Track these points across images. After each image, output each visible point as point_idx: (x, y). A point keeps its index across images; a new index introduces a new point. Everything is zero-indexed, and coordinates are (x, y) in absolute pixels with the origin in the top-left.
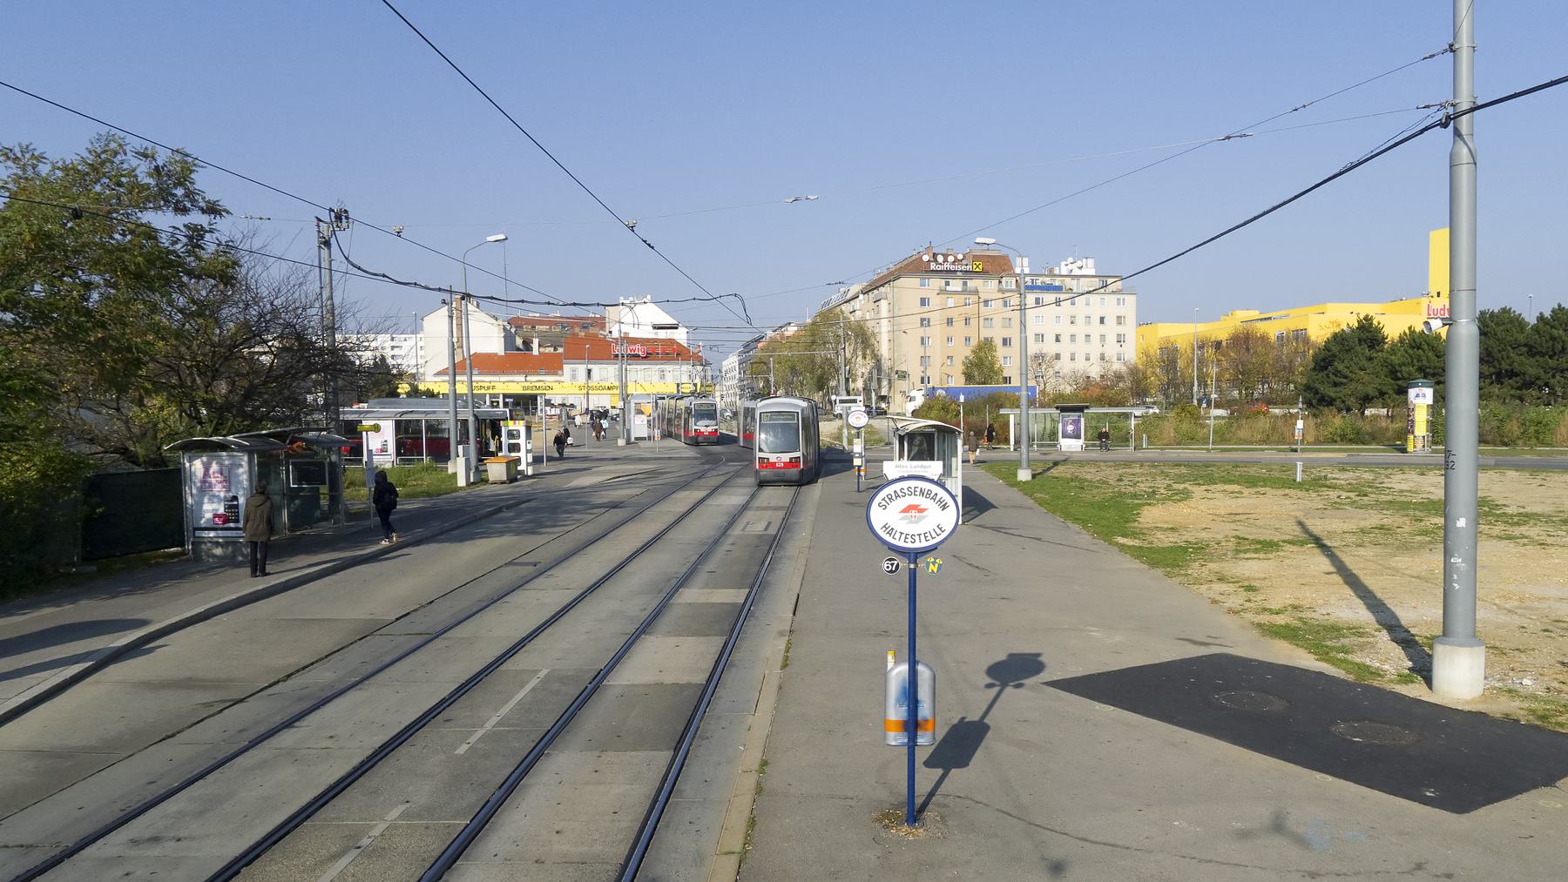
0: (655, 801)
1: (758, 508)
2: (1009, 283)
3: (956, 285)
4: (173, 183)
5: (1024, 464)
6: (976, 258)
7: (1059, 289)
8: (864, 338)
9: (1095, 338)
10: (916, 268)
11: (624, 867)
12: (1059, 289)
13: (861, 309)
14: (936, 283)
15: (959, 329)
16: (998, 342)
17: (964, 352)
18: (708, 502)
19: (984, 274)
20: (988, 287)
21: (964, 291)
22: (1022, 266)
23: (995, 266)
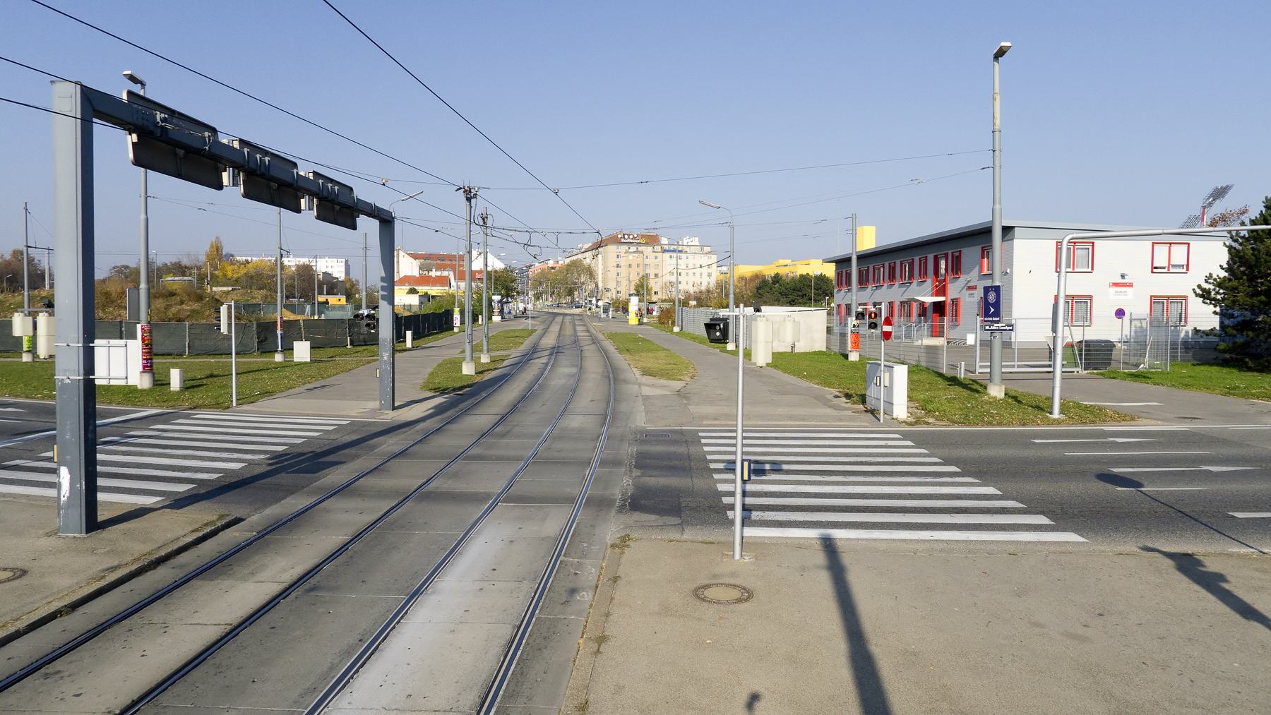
0: (372, 653)
1: (519, 459)
2: (658, 248)
3: (633, 249)
4: (692, 439)
5: (997, 378)
6: (643, 236)
7: (680, 251)
8: (591, 273)
9: (698, 274)
10: (615, 240)
11: (362, 666)
12: (680, 251)
13: (587, 259)
14: (624, 248)
15: (634, 270)
16: (652, 276)
17: (635, 279)
18: (348, 538)
19: (647, 244)
20: (648, 250)
21: (637, 252)
22: (664, 241)
23: (652, 240)
